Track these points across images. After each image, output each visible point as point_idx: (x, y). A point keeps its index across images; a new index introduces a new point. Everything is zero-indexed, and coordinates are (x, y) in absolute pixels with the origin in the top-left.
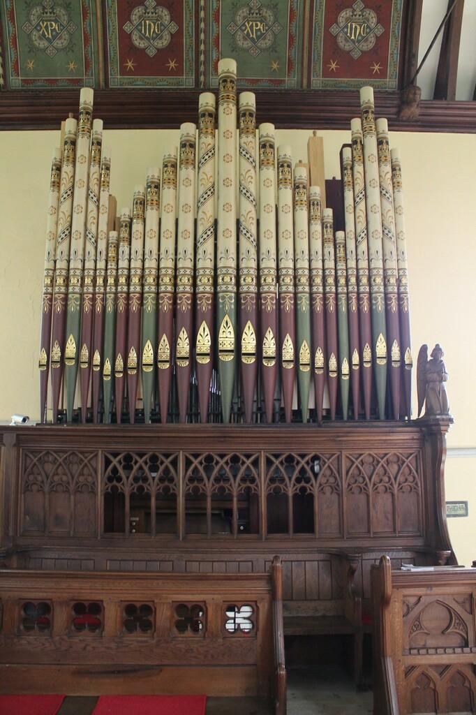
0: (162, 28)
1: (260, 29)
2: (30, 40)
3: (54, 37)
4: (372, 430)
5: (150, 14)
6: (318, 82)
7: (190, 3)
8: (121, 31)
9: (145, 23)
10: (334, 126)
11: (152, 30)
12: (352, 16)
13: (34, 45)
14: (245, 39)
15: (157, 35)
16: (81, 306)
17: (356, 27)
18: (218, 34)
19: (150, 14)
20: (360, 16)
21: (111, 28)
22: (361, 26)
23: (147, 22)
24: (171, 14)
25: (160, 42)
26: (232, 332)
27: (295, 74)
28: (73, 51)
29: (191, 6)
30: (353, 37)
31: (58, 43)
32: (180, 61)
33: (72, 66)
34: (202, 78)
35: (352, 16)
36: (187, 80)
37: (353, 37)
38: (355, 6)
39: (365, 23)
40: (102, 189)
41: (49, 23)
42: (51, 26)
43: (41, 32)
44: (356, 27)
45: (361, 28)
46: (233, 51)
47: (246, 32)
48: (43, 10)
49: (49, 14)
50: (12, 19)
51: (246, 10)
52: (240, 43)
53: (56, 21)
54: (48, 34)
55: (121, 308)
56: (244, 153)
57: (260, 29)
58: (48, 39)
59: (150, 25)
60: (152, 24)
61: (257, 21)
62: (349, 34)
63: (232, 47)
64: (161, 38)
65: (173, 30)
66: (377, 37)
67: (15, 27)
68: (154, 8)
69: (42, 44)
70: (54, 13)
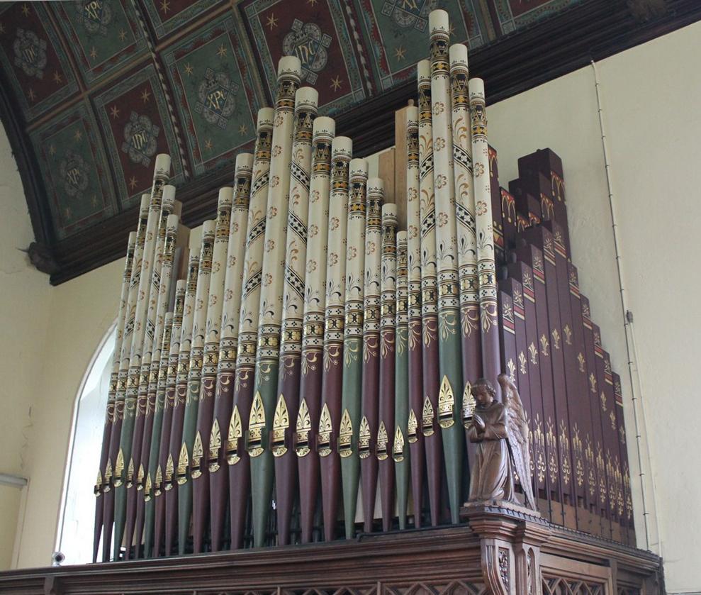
0: (316, 46)
1: (221, 97)
2: (203, 118)
3: (222, 106)
4: (464, 558)
5: (300, 37)
6: (509, 26)
7: (336, 4)
8: (121, 153)
9: (298, 49)
10: (113, 257)
11: (307, 54)
12: (295, 39)
13: (207, 122)
14: (405, 15)
15: (313, 56)
16: (458, 327)
17: (303, 49)
18: (375, 24)
19: (300, 37)
20: (302, 35)
21: (269, 72)
22: (307, 45)
23: (300, 47)
24: (319, 26)
25: (318, 63)
26: (263, 415)
27: (477, 30)
28: (241, 114)
29: (338, 9)
30: (139, 148)
31: (227, 111)
32: (343, 76)
33: (243, 129)
34: (369, 85)
35: (295, 39)
36: (357, 94)
37: (139, 148)
38: (294, 27)
39: (311, 40)
40: (349, 215)
41: (214, 94)
42: (217, 95)
43: (210, 107)
44: (303, 49)
45: (308, 48)
46: (396, 36)
47: (404, 6)
48: (208, 83)
49: (213, 85)
50: (186, 107)
51: (204, 84)
52: (401, 23)
53: (220, 89)
54: (413, 5)
55: (467, 329)
56: (459, 154)
57: (221, 97)
58: (414, 11)
59: (303, 49)
60: (305, 48)
61: (216, 91)
62: (136, 147)
63: (394, 32)
64: (318, 59)
65: (327, 44)
66: (156, 138)
67: (372, 16)
68: (303, 29)
69: (213, 119)
70: (217, 82)
